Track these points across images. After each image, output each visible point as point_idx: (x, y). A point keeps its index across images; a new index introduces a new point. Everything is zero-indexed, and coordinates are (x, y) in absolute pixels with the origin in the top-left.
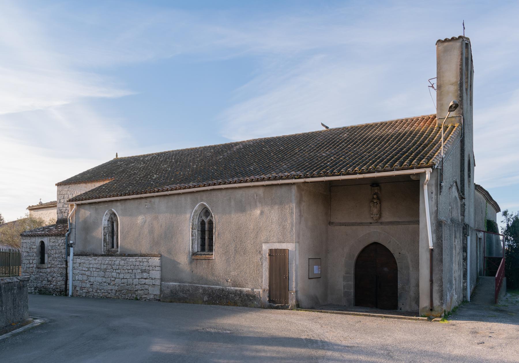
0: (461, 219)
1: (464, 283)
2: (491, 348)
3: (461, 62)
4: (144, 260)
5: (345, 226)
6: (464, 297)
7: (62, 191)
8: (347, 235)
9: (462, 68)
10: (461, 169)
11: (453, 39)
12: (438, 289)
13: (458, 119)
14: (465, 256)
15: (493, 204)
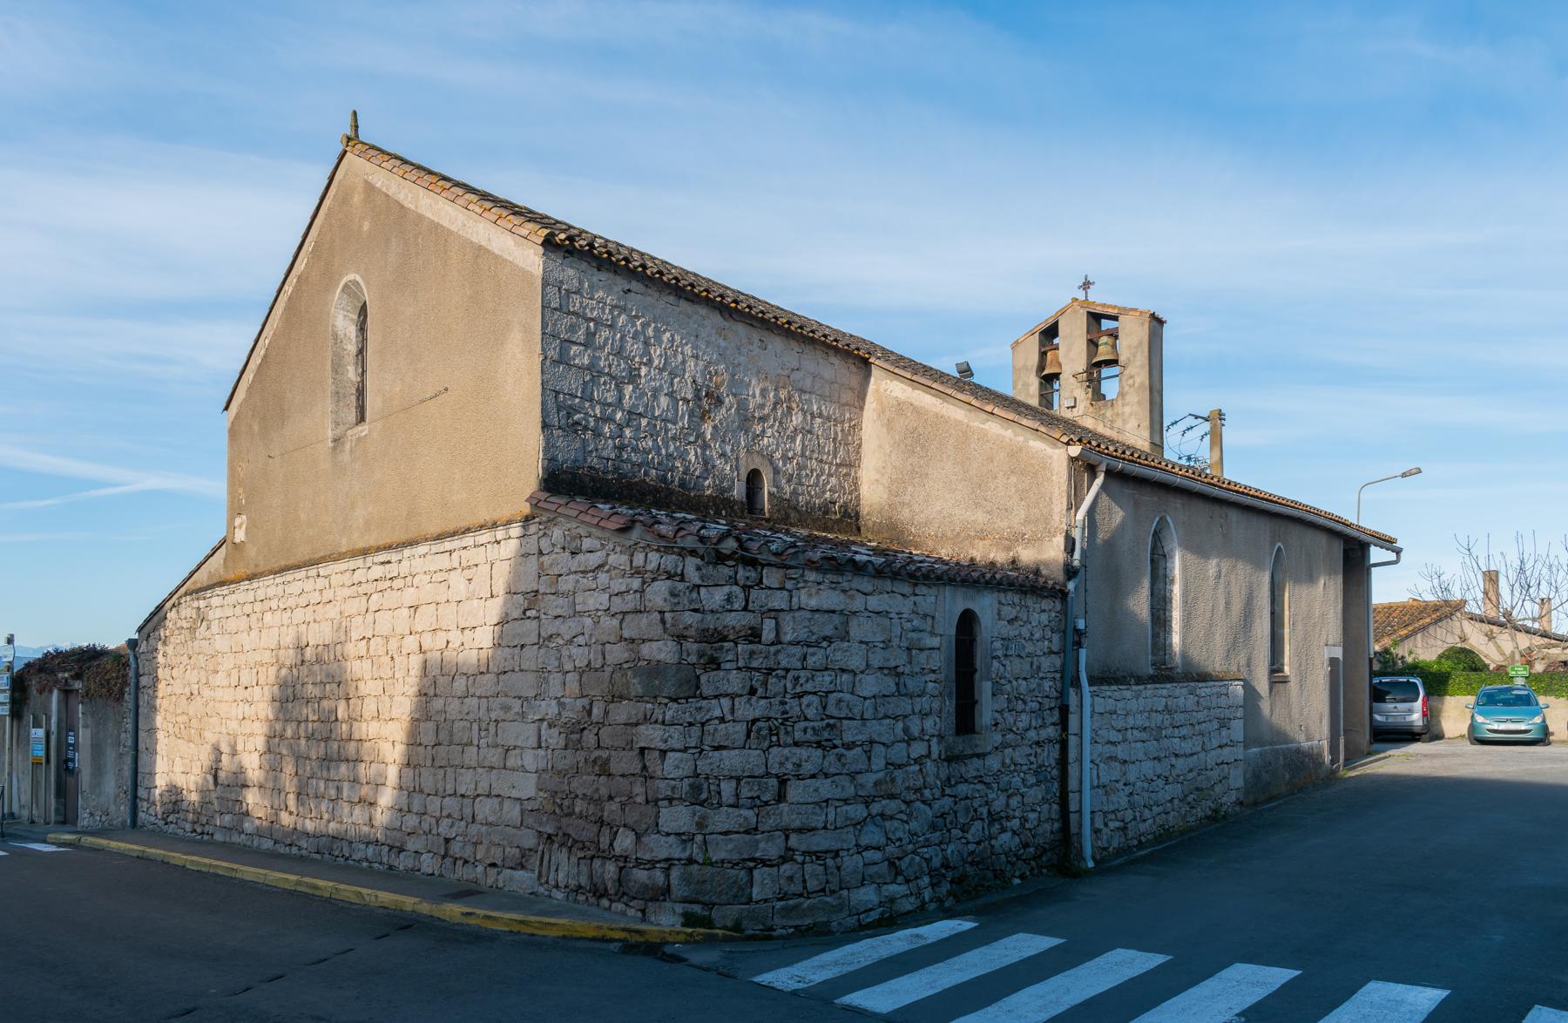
4: (1177, 692)
7: (578, 292)
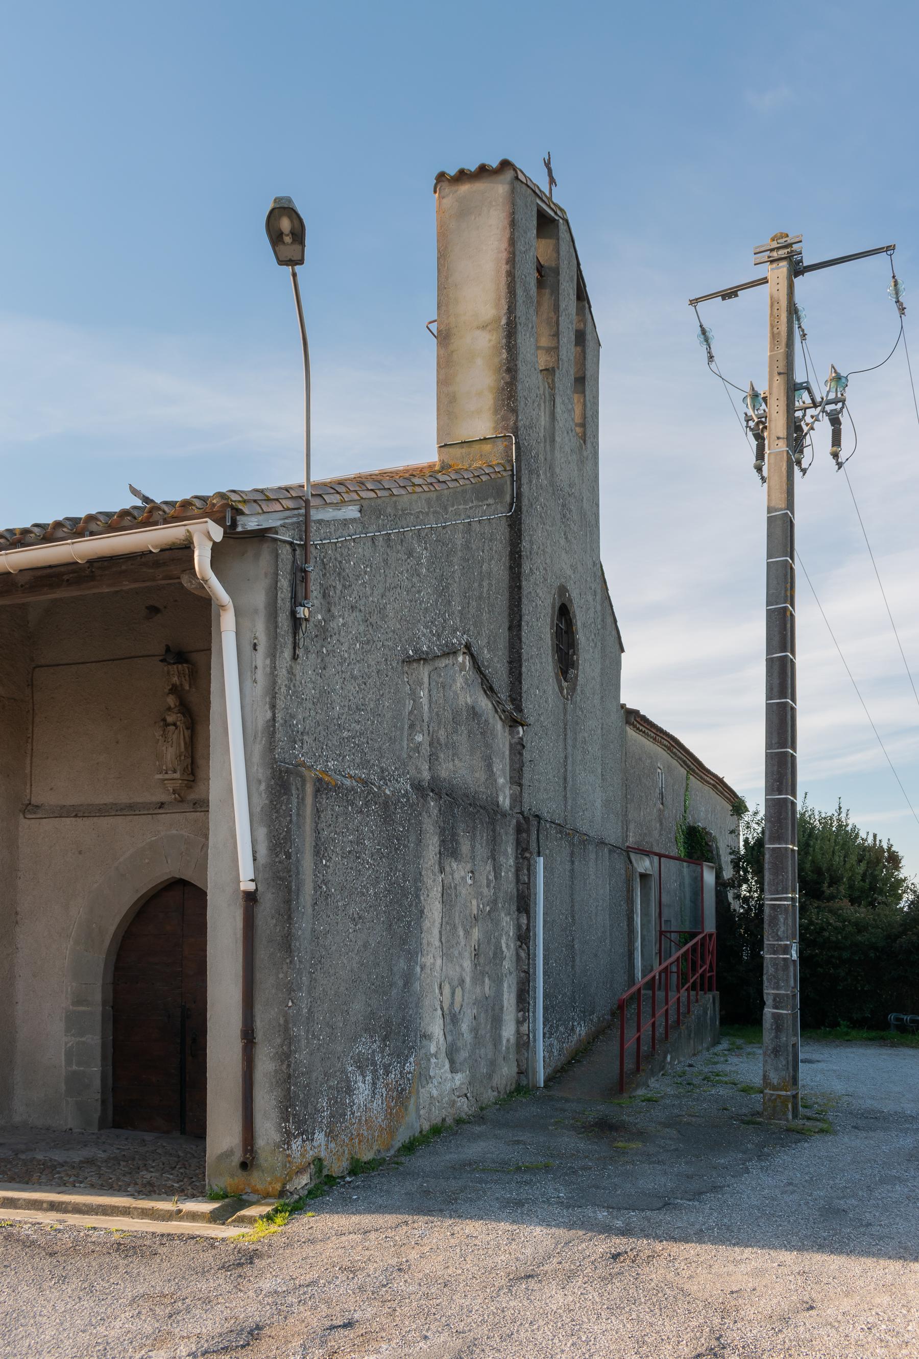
0: (511, 795)
1: (519, 1023)
2: (619, 1254)
3: (509, 253)
5: (76, 816)
6: (520, 1073)
8: (80, 853)
9: (512, 270)
10: (511, 621)
11: (483, 171)
12: (276, 1071)
13: (501, 446)
14: (524, 927)
15: (713, 785)
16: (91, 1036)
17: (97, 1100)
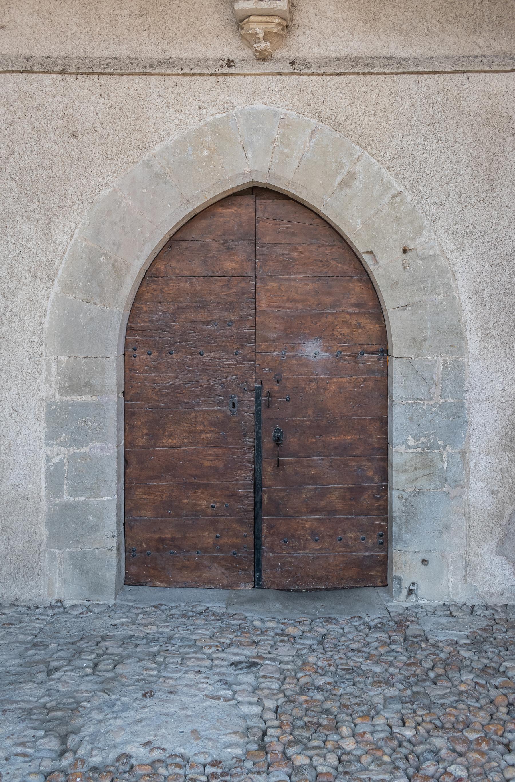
5: (63, 72)
8: (74, 135)
16: (98, 444)
17: (111, 550)
